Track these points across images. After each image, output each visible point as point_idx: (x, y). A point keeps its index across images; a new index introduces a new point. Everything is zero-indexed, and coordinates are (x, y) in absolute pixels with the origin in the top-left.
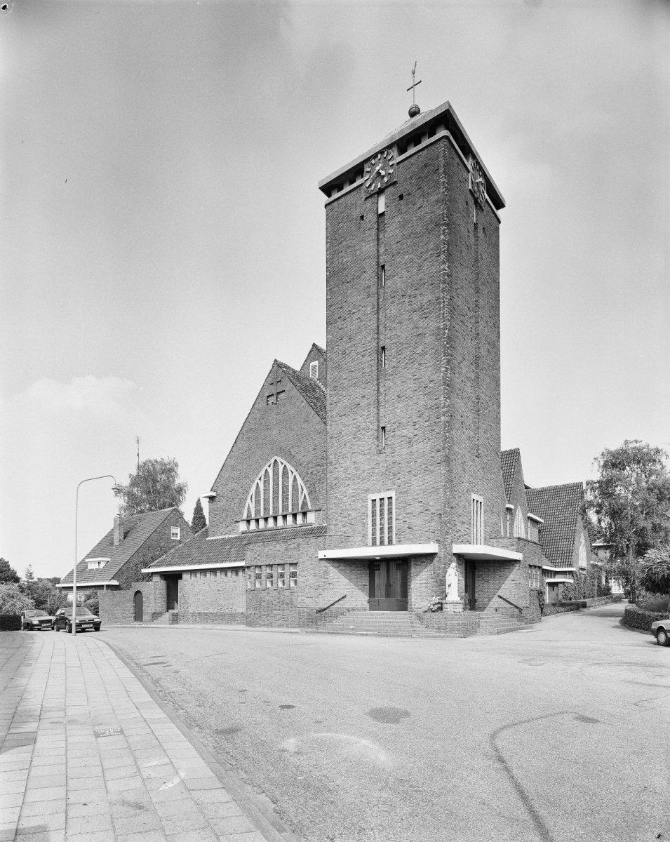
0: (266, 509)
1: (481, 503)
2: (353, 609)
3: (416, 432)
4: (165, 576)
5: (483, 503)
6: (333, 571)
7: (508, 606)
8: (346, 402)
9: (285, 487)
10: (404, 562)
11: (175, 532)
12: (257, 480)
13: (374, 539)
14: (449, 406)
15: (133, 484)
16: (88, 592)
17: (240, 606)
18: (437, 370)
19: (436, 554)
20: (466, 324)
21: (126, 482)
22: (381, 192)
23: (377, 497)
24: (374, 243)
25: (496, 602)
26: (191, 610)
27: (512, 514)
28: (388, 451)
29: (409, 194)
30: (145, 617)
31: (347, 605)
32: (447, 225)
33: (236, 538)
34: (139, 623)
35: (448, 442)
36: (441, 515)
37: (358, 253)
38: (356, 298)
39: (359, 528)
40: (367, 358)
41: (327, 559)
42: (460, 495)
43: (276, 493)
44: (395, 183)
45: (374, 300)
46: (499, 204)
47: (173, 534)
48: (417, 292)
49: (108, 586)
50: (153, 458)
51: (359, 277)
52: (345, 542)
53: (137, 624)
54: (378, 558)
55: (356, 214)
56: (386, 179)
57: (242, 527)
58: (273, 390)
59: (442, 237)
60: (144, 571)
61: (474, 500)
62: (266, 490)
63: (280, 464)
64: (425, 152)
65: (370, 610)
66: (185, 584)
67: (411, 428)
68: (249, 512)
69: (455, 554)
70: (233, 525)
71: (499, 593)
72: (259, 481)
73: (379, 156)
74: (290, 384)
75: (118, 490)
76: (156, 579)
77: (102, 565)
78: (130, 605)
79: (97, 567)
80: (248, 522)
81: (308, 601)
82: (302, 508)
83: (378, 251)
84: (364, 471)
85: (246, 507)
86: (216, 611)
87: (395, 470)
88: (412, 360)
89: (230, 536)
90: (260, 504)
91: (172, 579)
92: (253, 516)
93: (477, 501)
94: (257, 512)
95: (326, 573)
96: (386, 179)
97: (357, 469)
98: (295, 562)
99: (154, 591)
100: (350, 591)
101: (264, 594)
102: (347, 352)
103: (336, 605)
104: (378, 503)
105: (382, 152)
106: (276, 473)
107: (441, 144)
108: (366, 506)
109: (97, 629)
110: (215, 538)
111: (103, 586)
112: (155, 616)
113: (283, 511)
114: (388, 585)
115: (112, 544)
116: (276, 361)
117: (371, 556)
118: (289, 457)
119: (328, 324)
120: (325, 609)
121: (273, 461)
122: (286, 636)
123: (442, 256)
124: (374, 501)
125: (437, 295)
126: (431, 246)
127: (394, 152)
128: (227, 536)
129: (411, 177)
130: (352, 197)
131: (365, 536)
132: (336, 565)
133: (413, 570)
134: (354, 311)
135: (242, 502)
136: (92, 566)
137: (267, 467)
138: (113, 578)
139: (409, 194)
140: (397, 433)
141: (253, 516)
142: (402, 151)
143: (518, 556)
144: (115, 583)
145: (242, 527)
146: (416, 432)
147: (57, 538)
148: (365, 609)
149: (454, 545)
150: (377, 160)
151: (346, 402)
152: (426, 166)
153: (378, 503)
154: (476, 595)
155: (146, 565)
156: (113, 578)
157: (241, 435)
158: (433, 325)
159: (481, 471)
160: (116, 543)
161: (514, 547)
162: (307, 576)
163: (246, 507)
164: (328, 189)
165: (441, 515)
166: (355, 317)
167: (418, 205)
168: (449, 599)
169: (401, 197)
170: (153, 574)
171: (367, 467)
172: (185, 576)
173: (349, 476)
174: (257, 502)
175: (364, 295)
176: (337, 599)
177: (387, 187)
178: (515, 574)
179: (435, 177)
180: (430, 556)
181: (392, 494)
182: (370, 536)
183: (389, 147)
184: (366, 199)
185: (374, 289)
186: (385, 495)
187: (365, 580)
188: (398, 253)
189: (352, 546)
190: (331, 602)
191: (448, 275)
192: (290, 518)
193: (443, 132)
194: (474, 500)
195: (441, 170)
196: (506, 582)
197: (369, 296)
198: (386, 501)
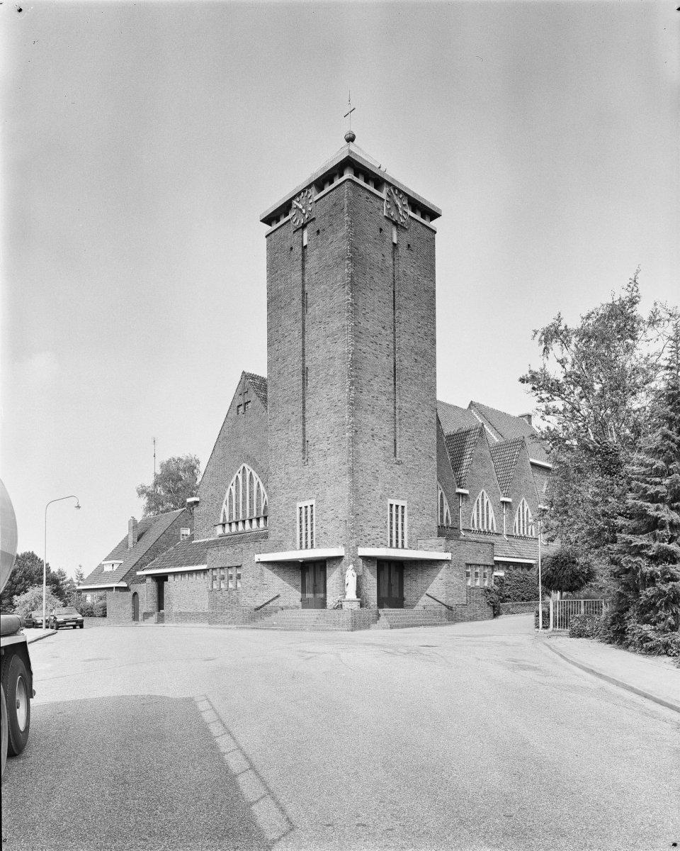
0: (251, 511)
1: (403, 507)
2: (287, 608)
3: (329, 446)
4: (154, 577)
5: (406, 508)
6: (269, 573)
7: (436, 603)
8: (281, 418)
9: (251, 492)
10: (320, 566)
11: (184, 533)
12: (230, 486)
13: (301, 546)
14: (352, 423)
15: (156, 484)
16: (101, 593)
17: (204, 605)
18: (343, 389)
19: (343, 556)
20: (379, 343)
21: (149, 481)
22: (304, 226)
23: (303, 504)
24: (300, 273)
25: (424, 600)
26: (175, 609)
27: (511, 508)
28: (310, 463)
29: (324, 230)
30: (141, 617)
31: (281, 604)
32: (351, 259)
33: (214, 541)
34: (136, 622)
35: (355, 457)
36: (346, 521)
37: (289, 281)
38: (288, 322)
39: (290, 534)
40: (295, 378)
41: (262, 562)
42: (369, 502)
43: (244, 498)
44: (314, 219)
45: (300, 325)
46: (433, 215)
47: (183, 535)
48: (329, 319)
49: (116, 588)
50: (177, 455)
51: (289, 303)
52: (279, 546)
53: (134, 623)
54: (301, 561)
55: (287, 245)
56: (307, 216)
57: (219, 530)
58: (241, 400)
59: (346, 270)
60: (139, 573)
61: (391, 505)
62: (237, 496)
63: (247, 470)
64: (334, 192)
65: (303, 607)
66: (171, 586)
67: (325, 443)
68: (225, 516)
69: (360, 557)
70: (212, 528)
71: (427, 592)
72: (232, 487)
73: (302, 194)
74: (254, 395)
75: (142, 492)
76: (149, 580)
77: (115, 567)
78: (129, 606)
79: (111, 569)
80: (224, 525)
81: (249, 601)
82: (264, 513)
83: (303, 281)
84: (293, 482)
85: (222, 511)
86: (192, 610)
87: (315, 480)
88: (327, 381)
89: (210, 539)
90: (232, 511)
91: (161, 580)
92: (227, 520)
93: (397, 506)
94: (231, 516)
95: (262, 574)
96: (307, 216)
97: (289, 479)
98: (239, 565)
99: (146, 591)
100: (287, 591)
101: (219, 594)
102: (282, 372)
103: (271, 604)
104: (303, 510)
105: (303, 191)
106: (244, 479)
107: (346, 185)
108: (295, 513)
109: (82, 627)
110: (198, 541)
111: (113, 588)
112: (147, 615)
113: (250, 515)
114: (315, 585)
115: (127, 547)
116: (244, 372)
117: (386, 556)
118: (254, 464)
119: (269, 345)
120: (261, 607)
121: (242, 468)
122: (226, 631)
123: (347, 288)
124: (301, 508)
125: (343, 323)
126: (339, 277)
127: (313, 191)
128: (207, 540)
129: (325, 215)
130: (269, 238)
131: (294, 540)
132: (271, 567)
133: (406, 573)
134: (286, 334)
135: (219, 506)
136: (108, 569)
137: (237, 474)
138: (122, 580)
139: (324, 230)
140: (317, 447)
141: (227, 520)
142: (320, 188)
143: (448, 556)
144: (124, 584)
145: (219, 530)
146: (329, 446)
147: (80, 543)
148: (297, 607)
149: (359, 549)
150: (301, 197)
151: (281, 418)
152: (335, 205)
153: (303, 510)
154: (405, 594)
155: (142, 567)
156: (122, 580)
157: (218, 443)
158: (340, 349)
159: (402, 476)
160: (131, 545)
161: (441, 547)
162: (248, 579)
163: (222, 511)
164: (268, 220)
165: (346, 521)
166: (287, 340)
167: (329, 241)
168: (348, 597)
169: (318, 232)
170: (147, 575)
171: (296, 478)
172: (170, 578)
173: (283, 486)
174: (231, 507)
175: (293, 321)
176: (271, 598)
177: (308, 222)
178: (443, 572)
179: (342, 215)
180: (339, 558)
181: (313, 502)
182: (298, 541)
183: (309, 187)
184: (294, 232)
185: (300, 315)
186: (308, 503)
187: (298, 581)
188: (317, 283)
189: (285, 550)
190: (266, 601)
191: (352, 305)
192: (254, 522)
193: (348, 175)
194: (391, 505)
195: (345, 210)
196: (435, 581)
197: (296, 321)
198: (309, 509)
